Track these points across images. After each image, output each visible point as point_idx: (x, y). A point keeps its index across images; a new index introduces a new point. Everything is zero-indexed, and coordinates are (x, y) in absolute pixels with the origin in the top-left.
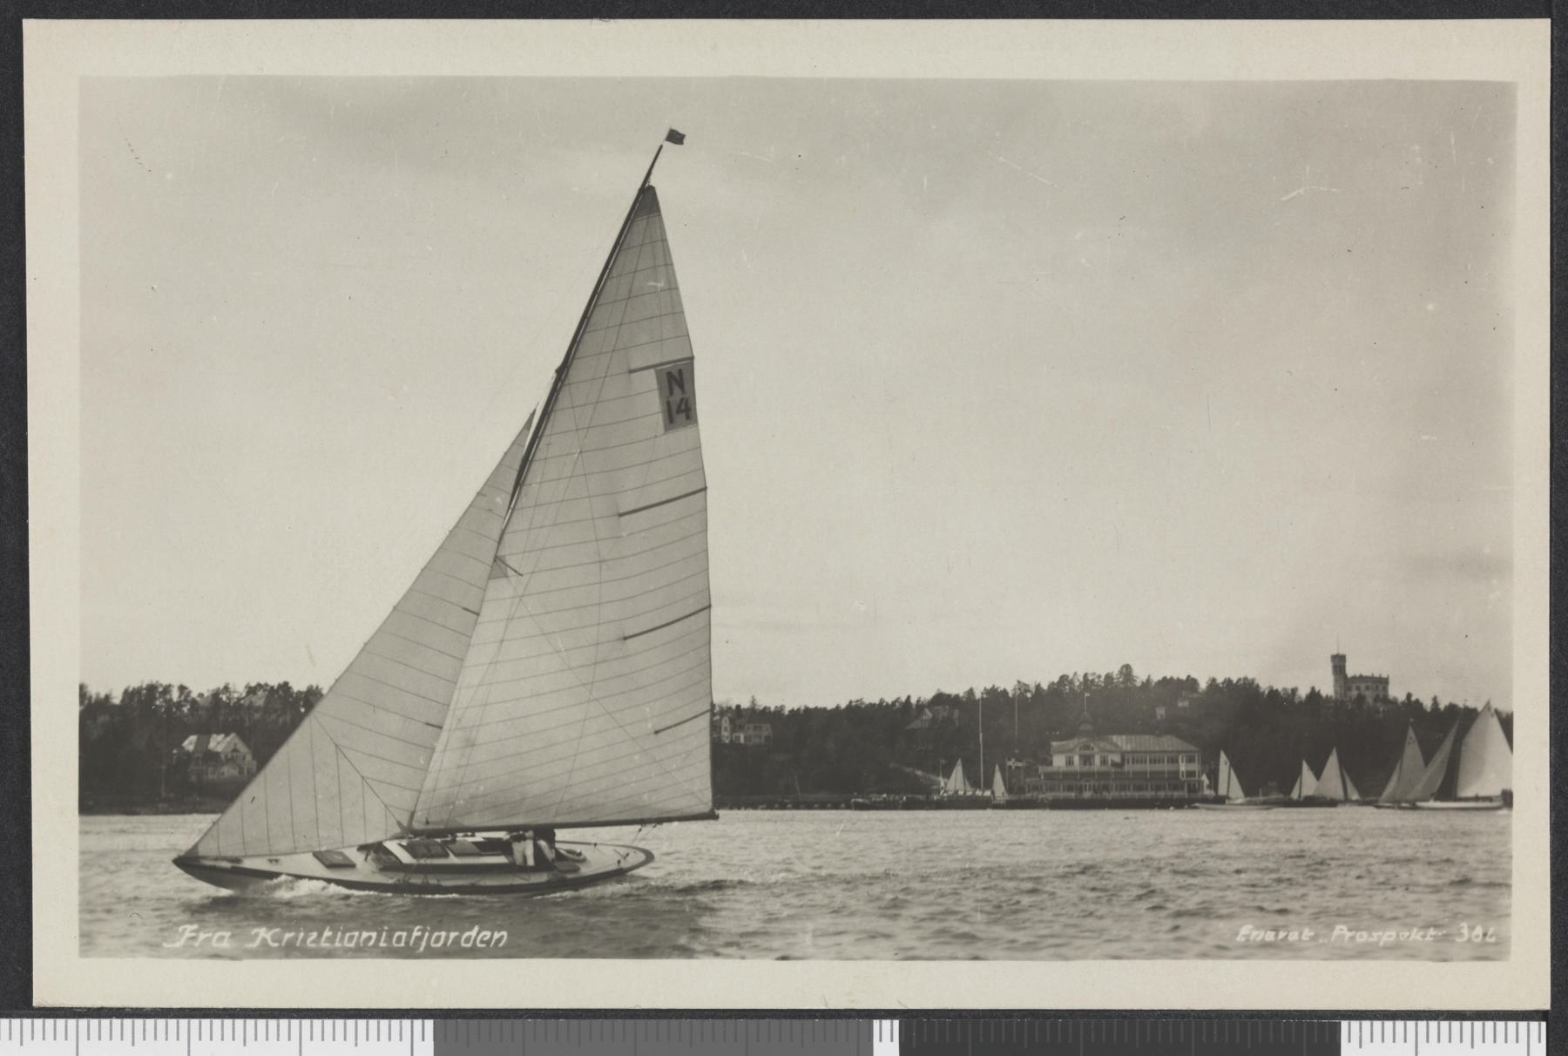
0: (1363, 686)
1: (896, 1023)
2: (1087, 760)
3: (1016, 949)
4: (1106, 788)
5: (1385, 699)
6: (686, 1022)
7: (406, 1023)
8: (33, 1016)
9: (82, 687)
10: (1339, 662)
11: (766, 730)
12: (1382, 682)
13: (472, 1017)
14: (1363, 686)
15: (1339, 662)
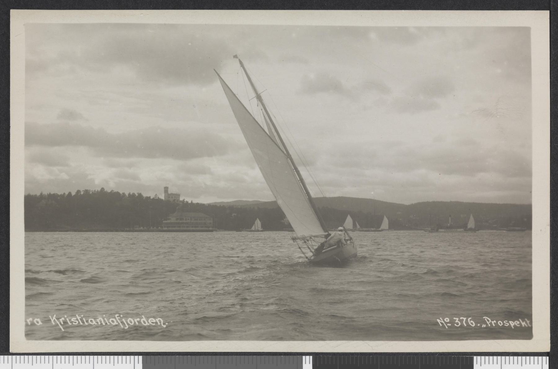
1: (311, 357)
3: (241, 338)
5: (178, 200)
6: (234, 357)
7: (132, 357)
10: (166, 189)
12: (178, 195)
13: (250, 355)
15: (166, 189)
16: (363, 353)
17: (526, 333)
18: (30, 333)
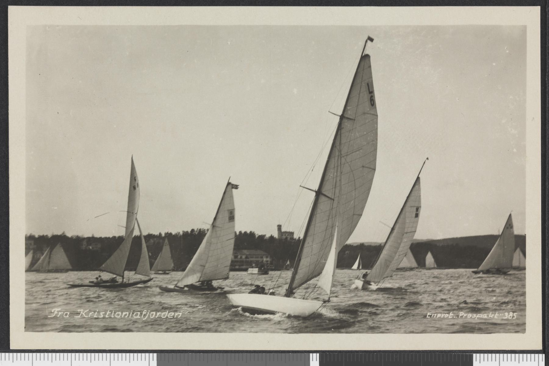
1: (318, 354)
4: (242, 265)
5: (292, 238)
7: (147, 354)
10: (279, 227)
11: (99, 246)
12: (292, 233)
15: (279, 227)
16: (368, 351)
17: (519, 327)
18: (34, 322)
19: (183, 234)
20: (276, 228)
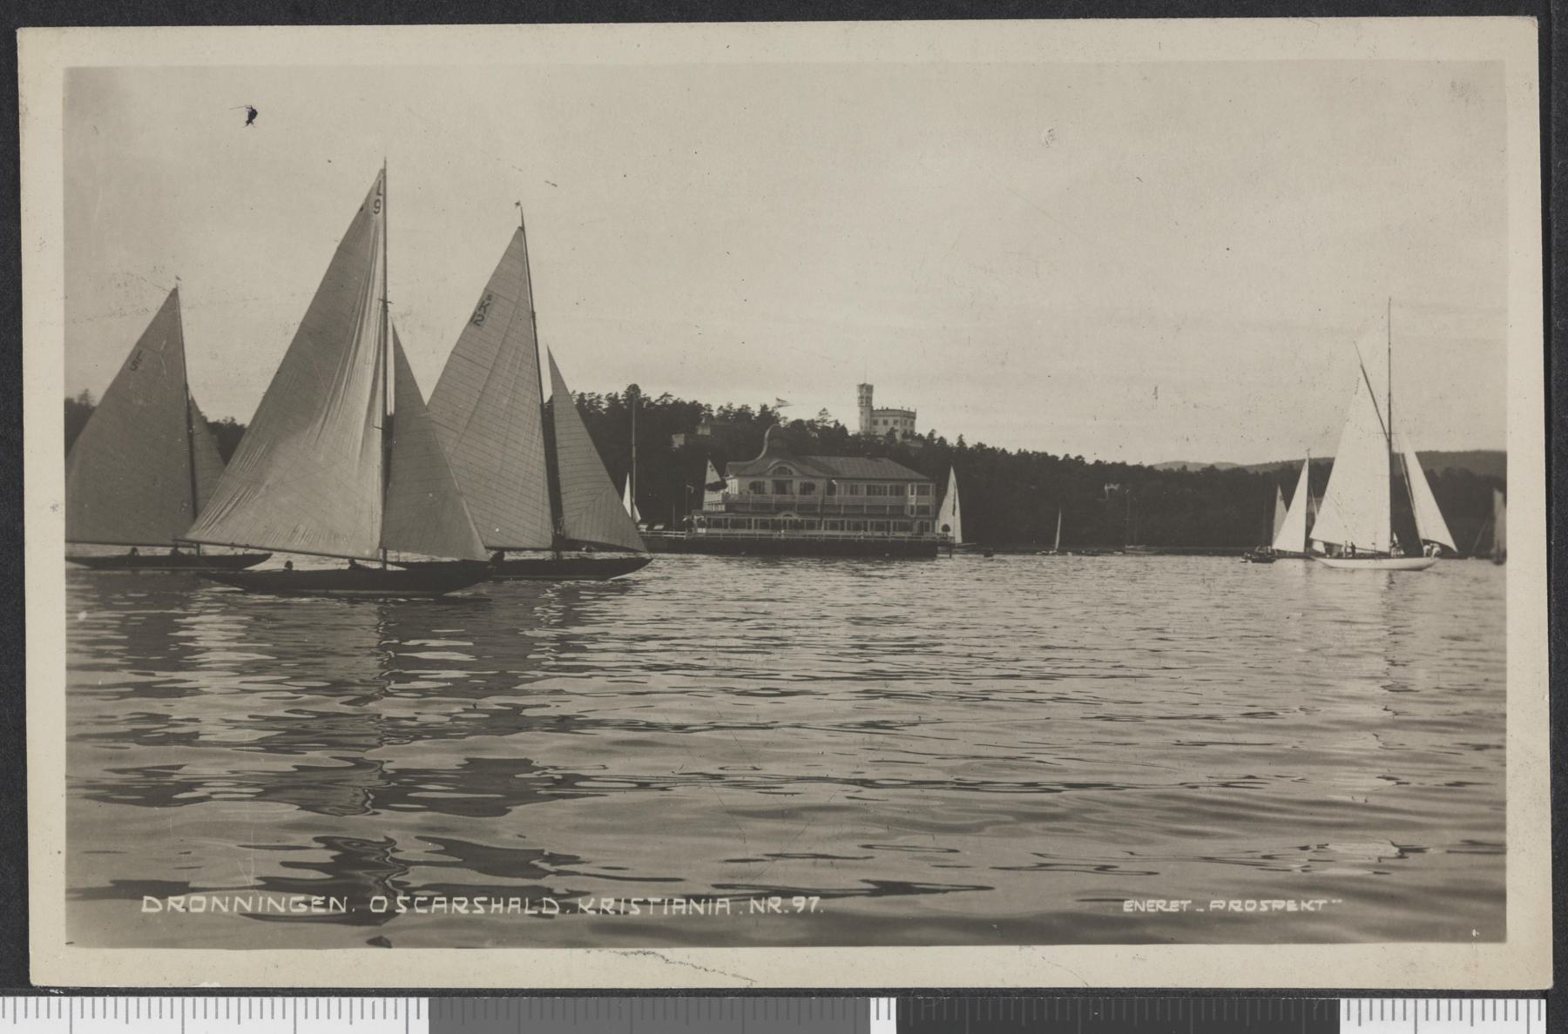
0: (891, 420)
1: (893, 1001)
2: (781, 488)
5: (909, 434)
7: (401, 1001)
8: (27, 994)
9: (174, 293)
10: (866, 391)
12: (910, 416)
14: (891, 420)
15: (866, 391)
17: (1494, 930)
18: (118, 896)
19: (720, 418)
20: (854, 396)
